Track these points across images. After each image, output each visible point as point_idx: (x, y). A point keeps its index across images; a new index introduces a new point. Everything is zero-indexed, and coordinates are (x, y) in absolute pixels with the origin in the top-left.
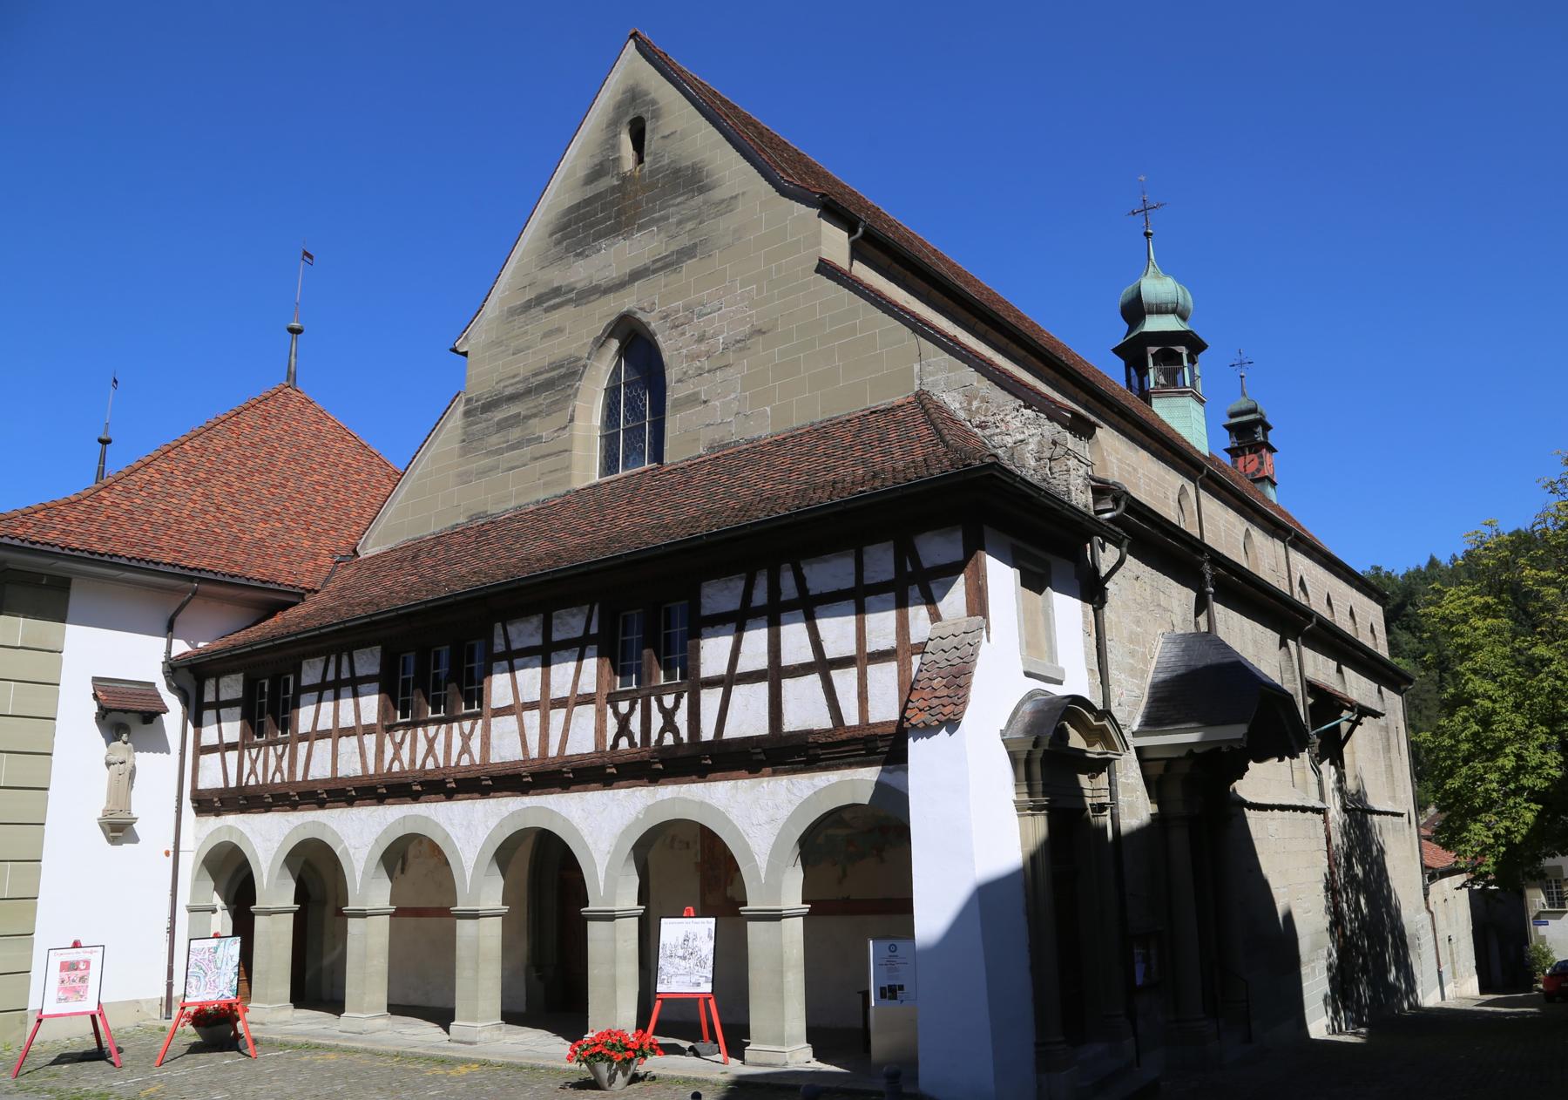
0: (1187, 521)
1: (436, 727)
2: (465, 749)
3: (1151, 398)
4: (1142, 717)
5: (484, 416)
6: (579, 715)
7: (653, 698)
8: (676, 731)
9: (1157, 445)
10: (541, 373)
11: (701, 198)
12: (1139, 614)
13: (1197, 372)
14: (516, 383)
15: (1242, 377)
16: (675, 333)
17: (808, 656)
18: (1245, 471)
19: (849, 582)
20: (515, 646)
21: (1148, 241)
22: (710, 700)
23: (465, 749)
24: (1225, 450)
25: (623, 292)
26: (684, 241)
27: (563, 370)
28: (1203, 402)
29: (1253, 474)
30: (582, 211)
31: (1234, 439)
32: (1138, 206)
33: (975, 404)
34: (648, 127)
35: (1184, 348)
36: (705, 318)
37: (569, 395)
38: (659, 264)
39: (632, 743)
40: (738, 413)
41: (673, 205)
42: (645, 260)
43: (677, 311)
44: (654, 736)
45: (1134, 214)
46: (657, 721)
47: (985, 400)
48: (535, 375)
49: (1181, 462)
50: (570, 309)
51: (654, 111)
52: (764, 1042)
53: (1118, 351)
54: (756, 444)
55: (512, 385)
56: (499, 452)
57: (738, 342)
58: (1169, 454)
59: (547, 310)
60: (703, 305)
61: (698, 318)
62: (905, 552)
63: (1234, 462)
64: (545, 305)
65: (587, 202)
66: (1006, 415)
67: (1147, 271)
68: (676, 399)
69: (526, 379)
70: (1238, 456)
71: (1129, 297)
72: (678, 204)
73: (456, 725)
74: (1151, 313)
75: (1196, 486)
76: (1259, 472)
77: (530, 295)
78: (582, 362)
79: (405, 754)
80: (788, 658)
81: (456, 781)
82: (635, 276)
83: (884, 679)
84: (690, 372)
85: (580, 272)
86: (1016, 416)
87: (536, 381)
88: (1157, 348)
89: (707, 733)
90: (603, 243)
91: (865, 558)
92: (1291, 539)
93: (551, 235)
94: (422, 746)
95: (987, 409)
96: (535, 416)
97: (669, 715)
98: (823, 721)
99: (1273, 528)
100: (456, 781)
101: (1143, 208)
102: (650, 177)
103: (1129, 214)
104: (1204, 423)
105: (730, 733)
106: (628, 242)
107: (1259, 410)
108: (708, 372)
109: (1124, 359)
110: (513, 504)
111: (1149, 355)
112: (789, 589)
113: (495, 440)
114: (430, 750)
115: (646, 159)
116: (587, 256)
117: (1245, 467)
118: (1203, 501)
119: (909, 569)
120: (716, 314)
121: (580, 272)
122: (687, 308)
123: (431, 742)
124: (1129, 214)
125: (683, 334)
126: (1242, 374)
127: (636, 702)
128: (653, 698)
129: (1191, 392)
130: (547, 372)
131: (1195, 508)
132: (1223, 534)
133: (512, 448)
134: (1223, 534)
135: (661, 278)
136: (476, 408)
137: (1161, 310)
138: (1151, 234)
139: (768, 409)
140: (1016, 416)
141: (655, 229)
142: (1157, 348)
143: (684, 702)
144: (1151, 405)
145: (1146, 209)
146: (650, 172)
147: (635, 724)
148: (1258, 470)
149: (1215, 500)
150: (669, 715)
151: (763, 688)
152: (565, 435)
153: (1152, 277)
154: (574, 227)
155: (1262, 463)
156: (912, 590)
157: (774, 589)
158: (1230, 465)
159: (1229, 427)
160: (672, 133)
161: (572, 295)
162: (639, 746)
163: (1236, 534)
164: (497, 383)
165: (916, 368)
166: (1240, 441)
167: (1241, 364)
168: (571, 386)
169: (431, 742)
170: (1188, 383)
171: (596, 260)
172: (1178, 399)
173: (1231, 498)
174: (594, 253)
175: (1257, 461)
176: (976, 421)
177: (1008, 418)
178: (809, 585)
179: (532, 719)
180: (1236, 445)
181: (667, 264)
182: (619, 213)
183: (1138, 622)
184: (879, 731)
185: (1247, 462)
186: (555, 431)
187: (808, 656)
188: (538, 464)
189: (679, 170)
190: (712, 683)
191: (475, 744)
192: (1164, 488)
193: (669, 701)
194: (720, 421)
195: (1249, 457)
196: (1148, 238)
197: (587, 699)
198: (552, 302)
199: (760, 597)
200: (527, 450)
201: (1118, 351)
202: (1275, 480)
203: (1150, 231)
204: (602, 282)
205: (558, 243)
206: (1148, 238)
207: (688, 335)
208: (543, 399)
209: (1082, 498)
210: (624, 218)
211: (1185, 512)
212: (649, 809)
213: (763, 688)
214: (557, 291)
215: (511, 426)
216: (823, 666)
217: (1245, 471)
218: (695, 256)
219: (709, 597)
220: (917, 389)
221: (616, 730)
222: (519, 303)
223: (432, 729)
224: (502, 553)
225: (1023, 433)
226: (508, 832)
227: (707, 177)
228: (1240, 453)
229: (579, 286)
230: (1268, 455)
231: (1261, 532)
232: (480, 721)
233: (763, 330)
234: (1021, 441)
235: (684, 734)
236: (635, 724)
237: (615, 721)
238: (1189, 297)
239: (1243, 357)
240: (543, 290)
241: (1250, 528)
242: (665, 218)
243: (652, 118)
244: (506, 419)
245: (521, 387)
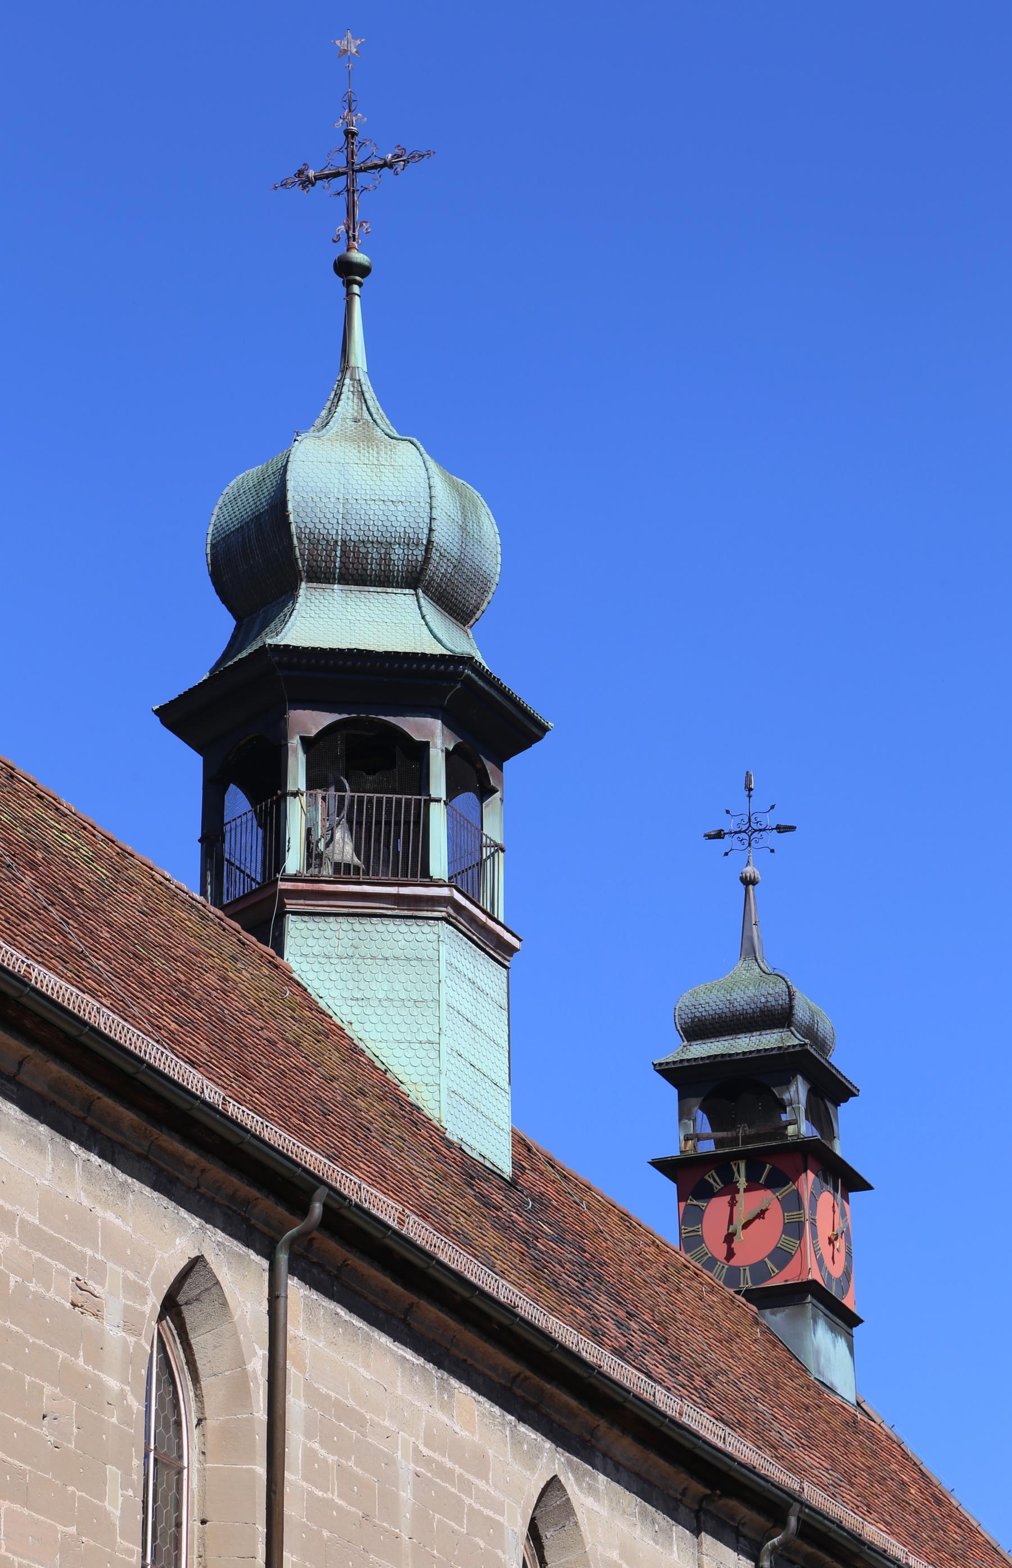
0: (210, 1423)
3: (282, 915)
9: (55, 1069)
13: (493, 828)
15: (748, 882)
18: (730, 1254)
21: (350, 295)
24: (869, 1187)
28: (510, 950)
29: (759, 1270)
31: (703, 1124)
35: (437, 725)
45: (307, 183)
49: (191, 1155)
58: (128, 1116)
63: (690, 1218)
67: (331, 412)
70: (706, 1193)
71: (246, 507)
74: (321, 576)
75: (273, 1270)
76: (781, 1266)
88: (328, 719)
92: (783, 1544)
99: (699, 1489)
101: (340, 162)
104: (502, 1038)
107: (801, 1013)
109: (198, 747)
111: (295, 743)
117: (729, 1238)
118: (296, 1328)
126: (750, 871)
129: (450, 901)
131: (258, 1364)
132: (406, 1494)
134: (406, 1494)
138: (364, 271)
142: (328, 719)
144: (279, 948)
145: (352, 170)
148: (781, 1257)
149: (385, 1340)
153: (345, 437)
155: (795, 1229)
158: (674, 1241)
159: (671, 1073)
163: (484, 1498)
166: (720, 1135)
167: (750, 831)
170: (439, 865)
172: (391, 925)
173: (469, 1337)
175: (776, 1216)
180: (708, 1147)
185: (740, 1219)
192: (76, 1260)
195: (748, 1202)
196: (348, 284)
202: (848, 1302)
203: (358, 257)
206: (348, 284)
211: (204, 1382)
217: (730, 1254)
228: (713, 1179)
230: (827, 1198)
231: (631, 1501)
238: (488, 529)
239: (760, 802)
241: (569, 1482)
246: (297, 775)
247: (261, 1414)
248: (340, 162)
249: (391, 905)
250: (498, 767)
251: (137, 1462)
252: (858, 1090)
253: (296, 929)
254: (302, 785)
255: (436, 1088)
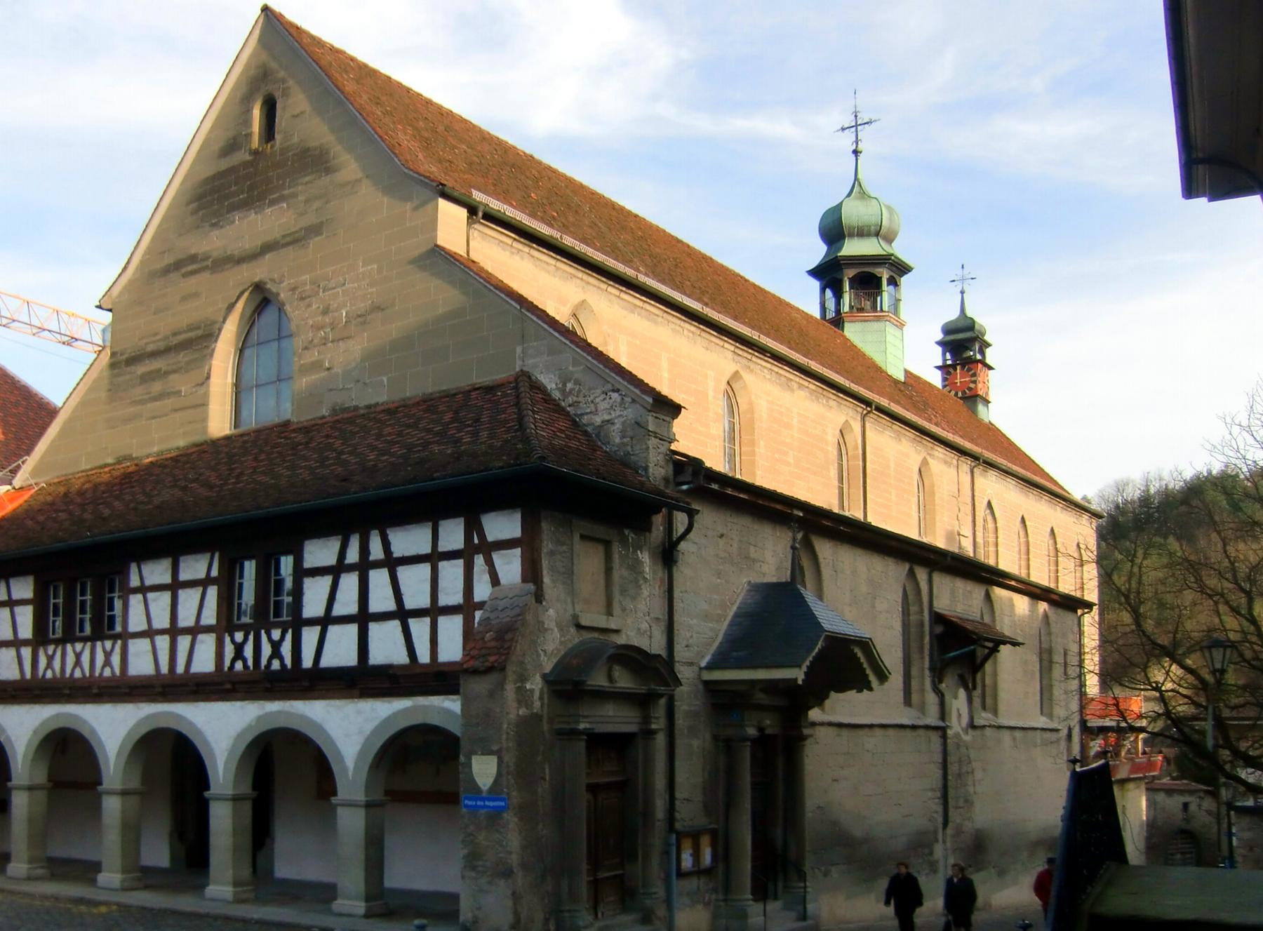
1: (82, 644)
2: (107, 663)
4: (713, 655)
5: (128, 369)
6: (202, 642)
7: (263, 632)
8: (282, 659)
10: (180, 333)
11: (328, 179)
12: (721, 567)
14: (158, 341)
16: (302, 304)
17: (391, 606)
19: (426, 549)
20: (148, 583)
22: (310, 636)
23: (107, 663)
25: (254, 263)
26: (311, 219)
27: (200, 332)
30: (216, 184)
32: (849, 121)
33: (569, 386)
34: (278, 106)
36: (330, 292)
37: (205, 356)
38: (288, 239)
39: (245, 666)
40: (358, 381)
41: (302, 184)
42: (276, 234)
43: (305, 284)
44: (264, 661)
46: (267, 650)
47: (577, 382)
48: (175, 334)
50: (206, 275)
51: (284, 90)
52: (348, 898)
53: (816, 273)
54: (373, 410)
55: (154, 342)
56: (142, 402)
57: (359, 316)
59: (185, 275)
60: (328, 280)
61: (323, 292)
62: (473, 527)
64: (183, 270)
65: (220, 175)
66: (596, 397)
68: (302, 365)
69: (166, 338)
72: (306, 183)
73: (99, 644)
74: (851, 235)
77: (169, 260)
78: (217, 326)
79: (57, 664)
80: (375, 606)
81: (99, 688)
82: (267, 248)
83: (451, 628)
84: (315, 341)
85: (215, 242)
86: (604, 399)
87: (175, 340)
89: (307, 662)
90: (237, 216)
91: (440, 529)
93: (188, 204)
94: (71, 659)
95: (579, 391)
96: (175, 371)
97: (276, 646)
98: (401, 658)
100: (99, 688)
102: (281, 155)
103: (838, 131)
105: (325, 662)
106: (259, 217)
108: (332, 342)
110: (155, 449)
111: (846, 278)
112: (376, 552)
113: (138, 392)
114: (78, 663)
115: (277, 136)
116: (222, 227)
119: (476, 541)
120: (339, 289)
121: (215, 242)
122: (313, 282)
123: (78, 656)
124: (838, 131)
125: (309, 305)
127: (249, 633)
128: (263, 632)
130: (185, 332)
133: (155, 399)
135: (290, 252)
136: (120, 362)
137: (862, 233)
139: (385, 379)
140: (604, 399)
141: (285, 205)
143: (289, 636)
144: (843, 330)
145: (856, 126)
146: (281, 150)
147: (249, 651)
150: (276, 646)
151: (353, 629)
152: (201, 391)
154: (209, 198)
156: (478, 558)
157: (364, 550)
160: (302, 113)
161: (209, 263)
162: (251, 668)
164: (140, 340)
165: (519, 350)
168: (207, 347)
169: (78, 656)
171: (229, 231)
174: (228, 224)
176: (570, 400)
177: (597, 400)
178: (393, 549)
179: (163, 642)
181: (295, 240)
182: (251, 188)
183: (719, 574)
184: (446, 669)
186: (194, 387)
187: (391, 606)
188: (178, 415)
189: (308, 149)
190: (312, 622)
191: (116, 659)
193: (276, 634)
194: (341, 387)
197: (208, 629)
198: (190, 268)
199: (353, 556)
200: (169, 403)
201: (816, 273)
204: (236, 253)
205: (194, 212)
207: (314, 307)
208: (183, 357)
209: (657, 471)
210: (256, 193)
212: (260, 719)
213: (353, 629)
214: (193, 258)
215: (153, 380)
216: (402, 614)
218: (321, 234)
219: (310, 553)
220: (518, 369)
221: (233, 655)
222: (158, 267)
223: (79, 646)
224: (141, 497)
225: (610, 414)
226: (144, 730)
227: (334, 158)
229: (215, 254)
232: (119, 642)
233: (382, 307)
234: (608, 421)
235: (288, 661)
236: (249, 651)
237: (232, 647)
240: (181, 256)
242: (294, 195)
243: (282, 97)
244: (150, 373)
245: (162, 345)
246: (847, 286)
247: (861, 452)
248: (859, 128)
249: (957, 650)
250: (911, 374)
251: (670, 318)
252: (890, 674)
253: (847, 325)
254: (848, 289)
255: (978, 722)
